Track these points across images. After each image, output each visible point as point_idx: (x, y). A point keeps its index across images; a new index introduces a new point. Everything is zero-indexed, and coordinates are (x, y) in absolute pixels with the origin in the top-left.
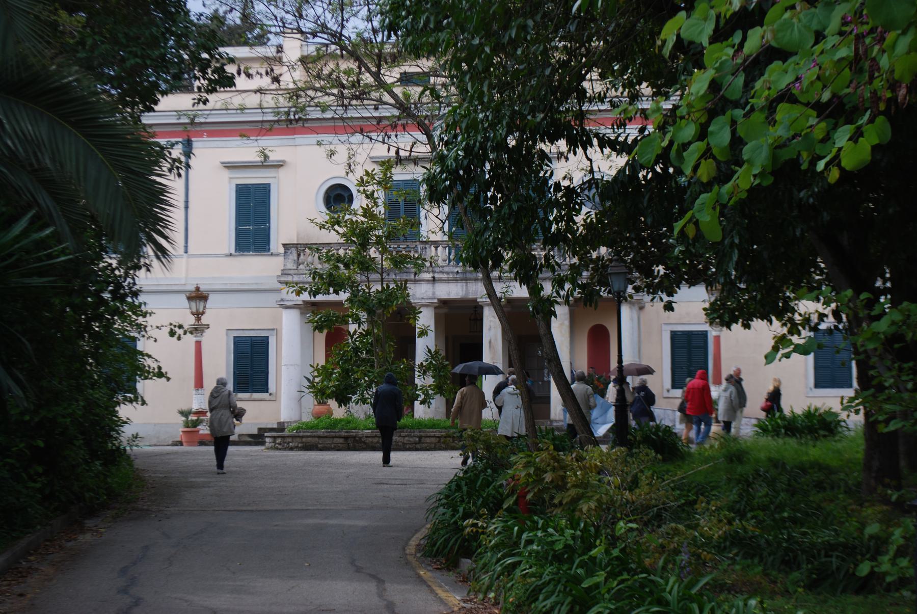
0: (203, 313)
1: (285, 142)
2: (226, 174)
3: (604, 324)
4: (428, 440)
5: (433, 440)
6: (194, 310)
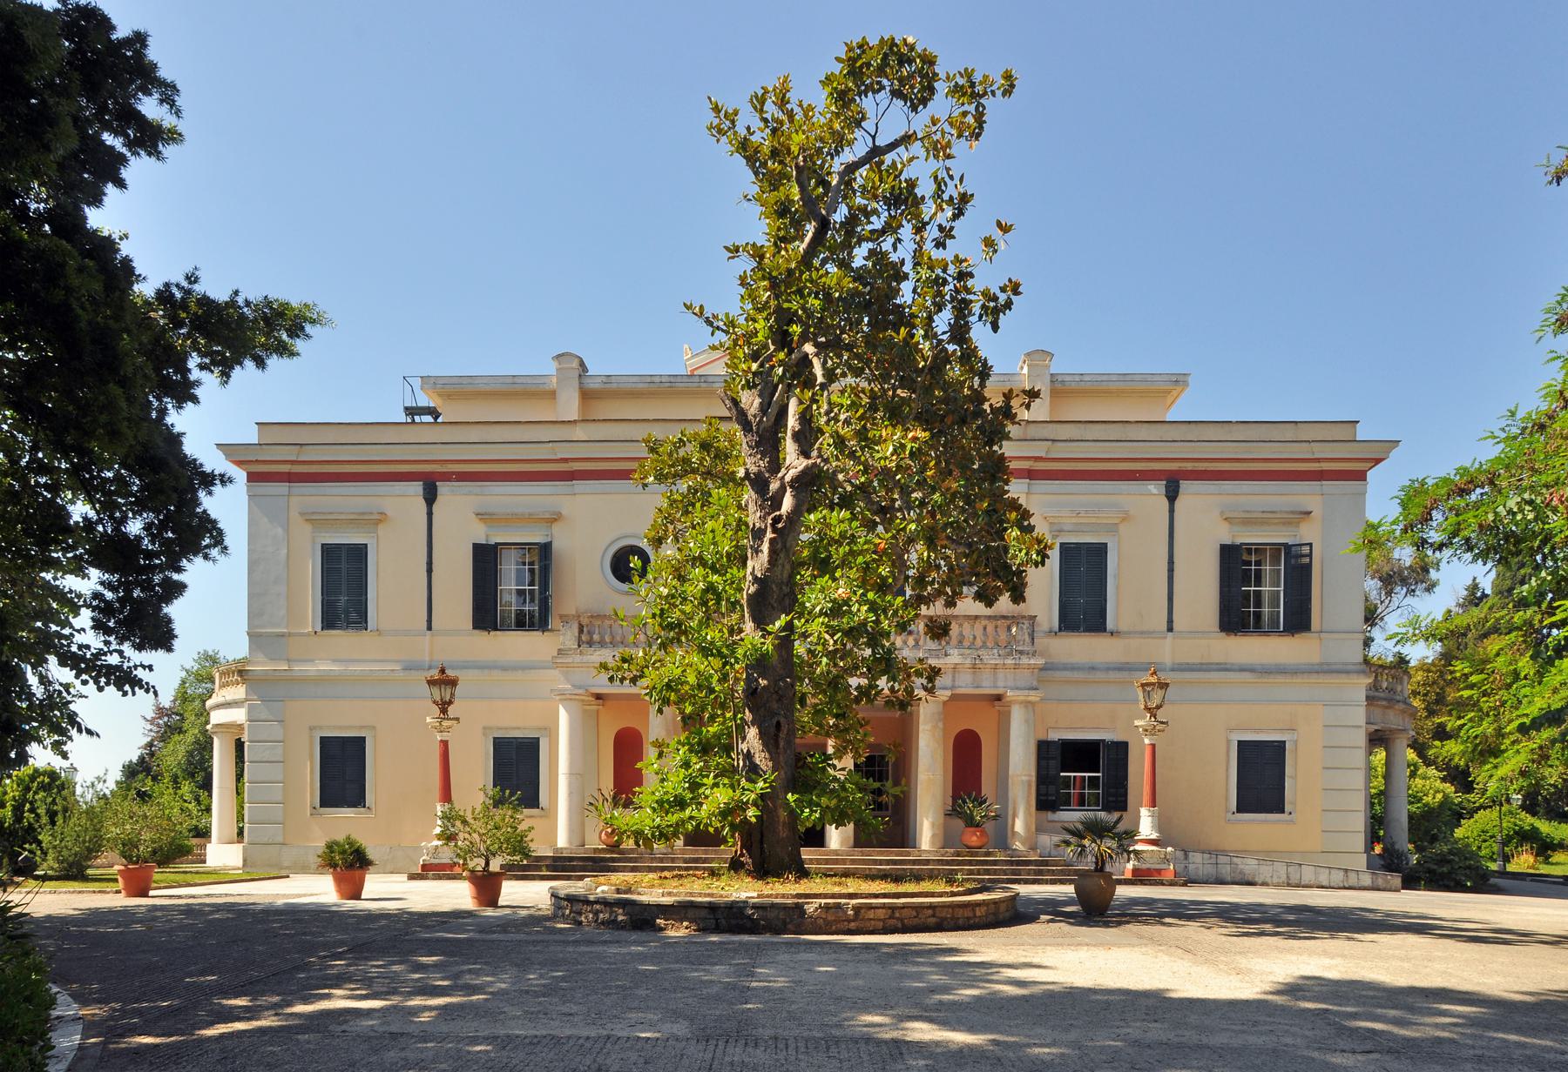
0: (450, 703)
4: (871, 914)
5: (881, 913)
6: (438, 699)
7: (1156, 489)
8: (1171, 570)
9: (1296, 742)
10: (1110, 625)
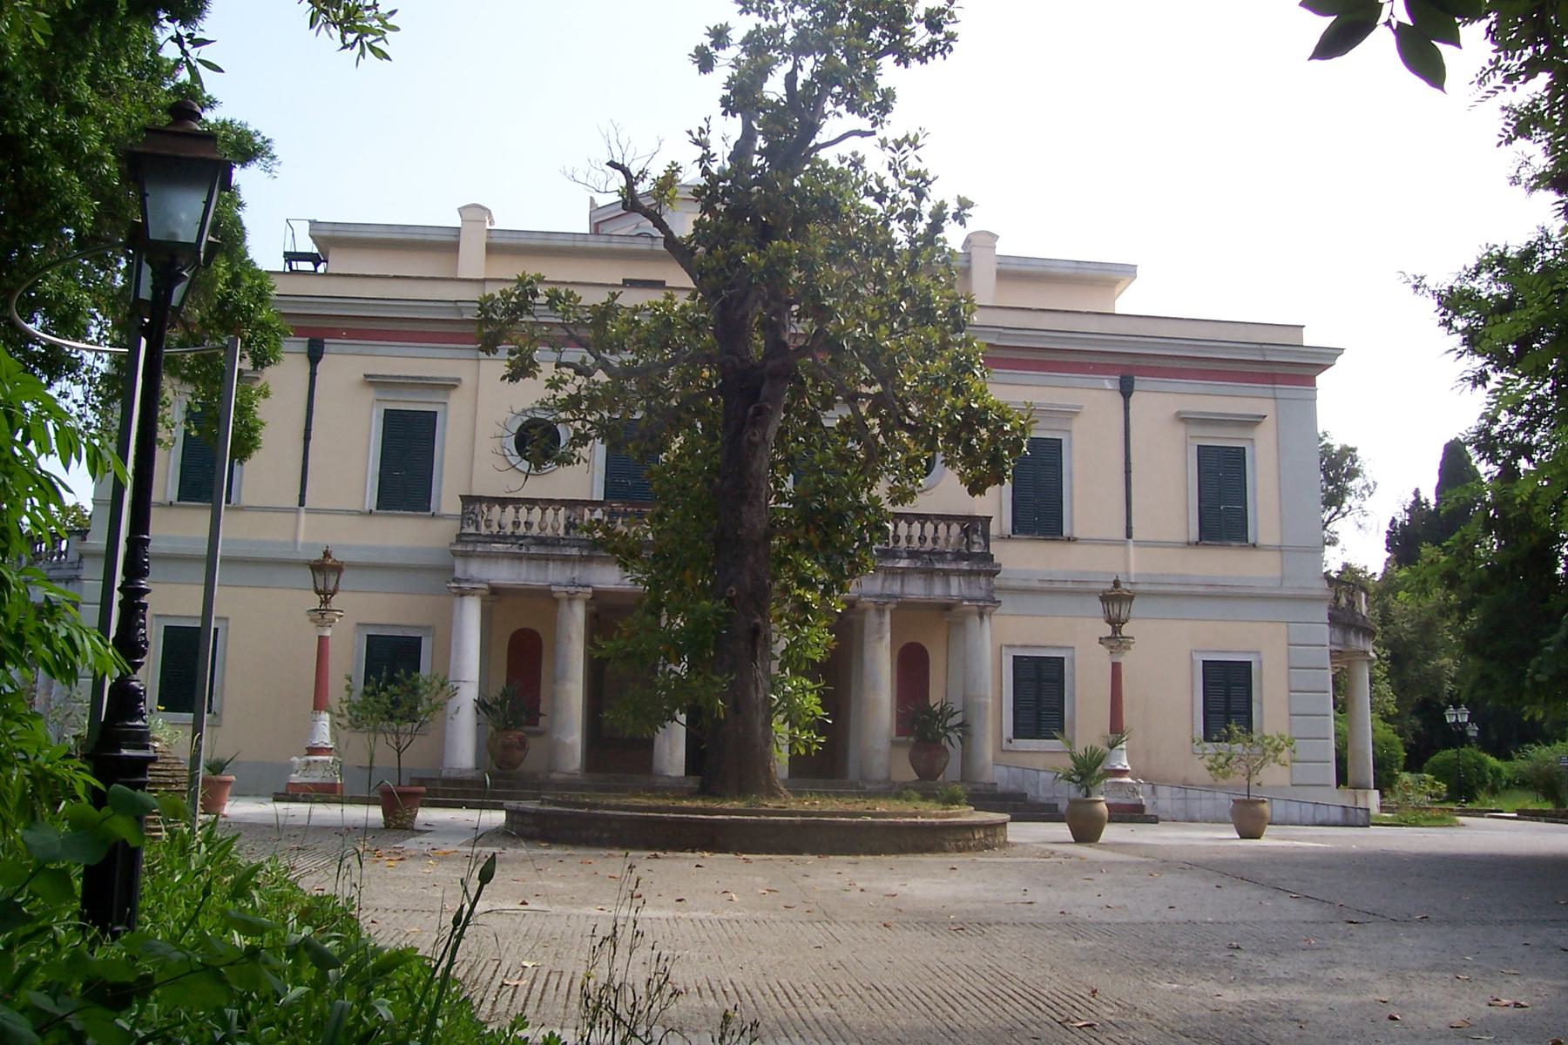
1: (456, 353)
2: (371, 394)
3: (927, 648)
7: (1110, 383)
8: (1128, 472)
9: (1261, 663)
10: (1066, 532)
